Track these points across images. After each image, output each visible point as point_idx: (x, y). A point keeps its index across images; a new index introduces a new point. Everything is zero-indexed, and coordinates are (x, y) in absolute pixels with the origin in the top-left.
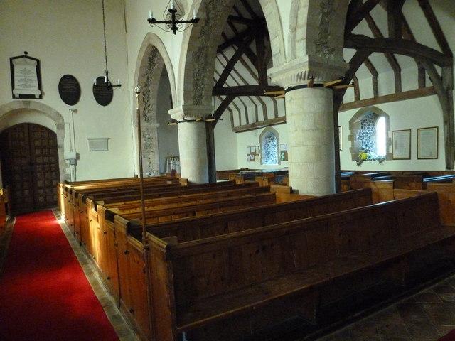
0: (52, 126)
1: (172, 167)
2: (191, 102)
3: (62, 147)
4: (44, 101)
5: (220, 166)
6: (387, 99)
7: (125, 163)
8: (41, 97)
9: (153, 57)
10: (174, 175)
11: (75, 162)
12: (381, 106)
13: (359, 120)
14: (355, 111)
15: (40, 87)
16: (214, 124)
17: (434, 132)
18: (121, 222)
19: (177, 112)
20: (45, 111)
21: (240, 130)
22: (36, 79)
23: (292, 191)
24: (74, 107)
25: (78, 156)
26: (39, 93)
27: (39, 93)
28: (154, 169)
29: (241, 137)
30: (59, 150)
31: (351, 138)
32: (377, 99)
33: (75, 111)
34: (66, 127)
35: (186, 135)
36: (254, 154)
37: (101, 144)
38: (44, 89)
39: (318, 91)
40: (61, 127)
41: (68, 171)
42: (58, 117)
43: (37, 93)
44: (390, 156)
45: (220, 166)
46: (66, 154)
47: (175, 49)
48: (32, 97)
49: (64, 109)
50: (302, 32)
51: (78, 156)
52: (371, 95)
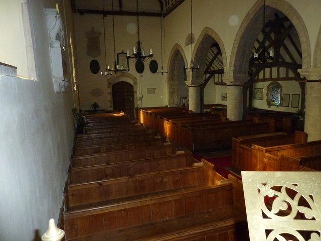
0: (131, 82)
1: (183, 103)
2: (194, 79)
3: (136, 92)
4: (130, 72)
5: (205, 103)
6: (282, 79)
7: (164, 99)
8: (128, 71)
9: (177, 55)
10: (185, 107)
11: (141, 99)
12: (280, 82)
13: (272, 86)
14: (270, 82)
15: (128, 67)
16: (204, 87)
17: (298, 96)
18: (180, 125)
19: (188, 82)
20: (130, 76)
21: (217, 84)
22: (127, 62)
23: (227, 119)
24: (142, 74)
25: (142, 96)
26: (128, 69)
27: (128, 69)
28: (176, 103)
29: (218, 87)
30: (135, 94)
31: (267, 94)
32: (279, 79)
33: (142, 76)
34: (138, 83)
35: (192, 93)
36: (224, 97)
37: (152, 91)
38: (130, 67)
39: (237, 87)
40: (136, 83)
41: (138, 103)
42: (135, 79)
43: (127, 69)
44: (281, 105)
45: (205, 103)
46: (138, 95)
47: (189, 55)
48: (125, 70)
49: (137, 75)
50: (232, 68)
51: (142, 96)
52: (277, 77)
